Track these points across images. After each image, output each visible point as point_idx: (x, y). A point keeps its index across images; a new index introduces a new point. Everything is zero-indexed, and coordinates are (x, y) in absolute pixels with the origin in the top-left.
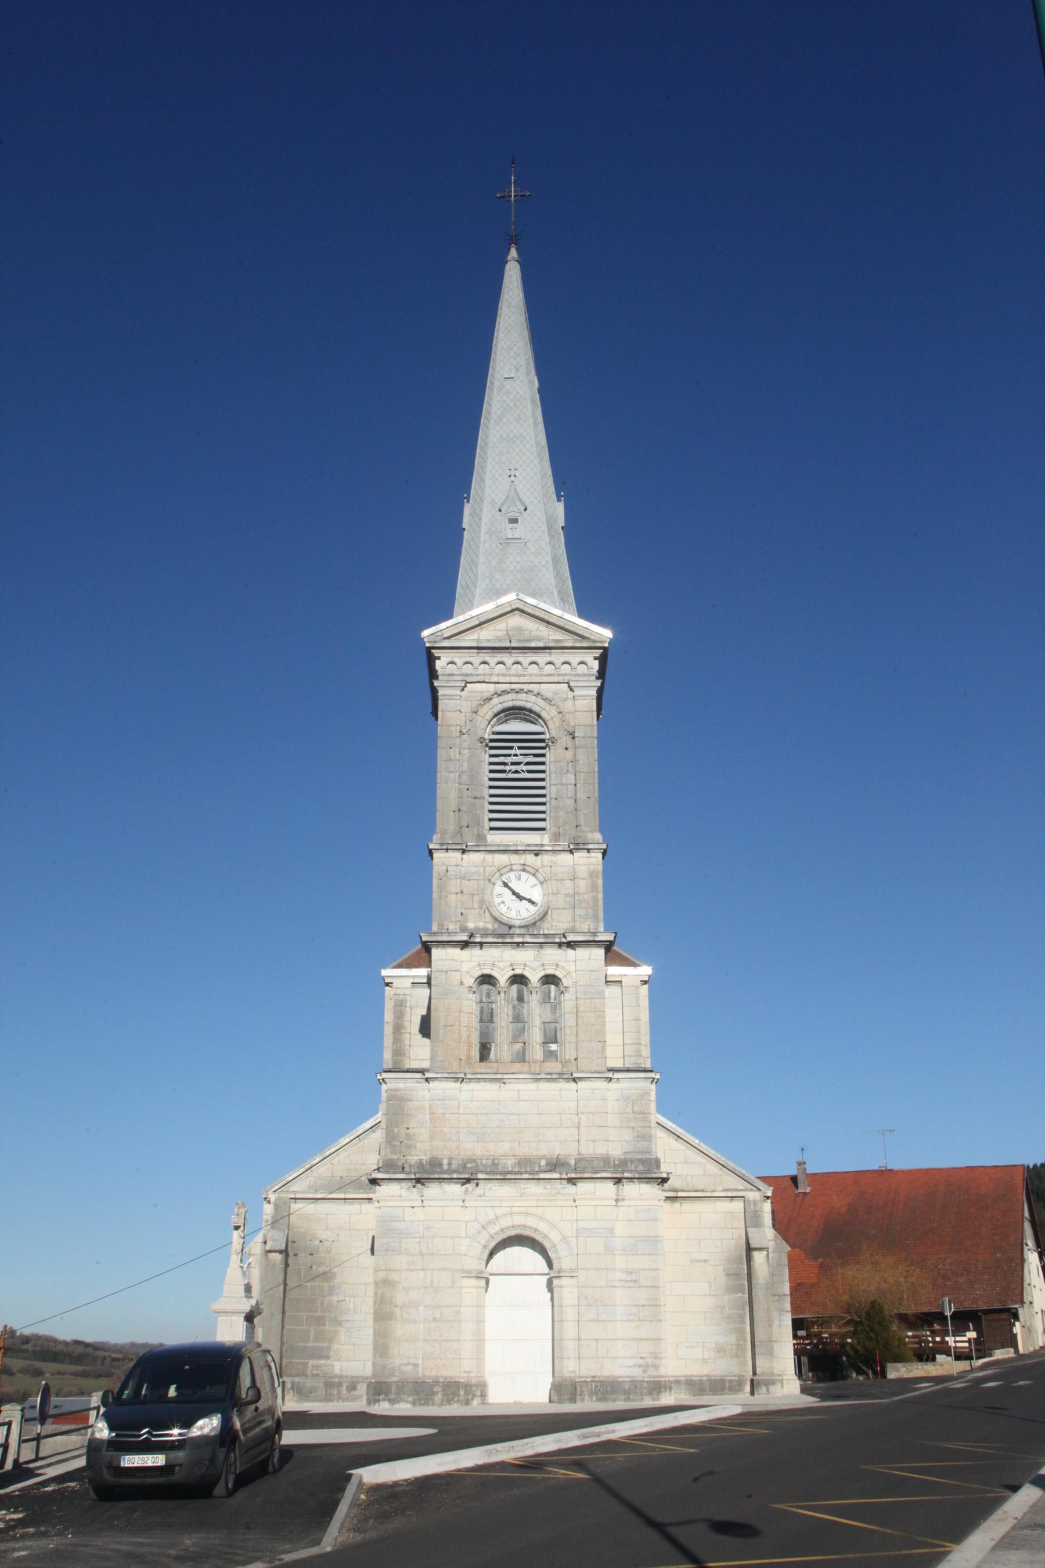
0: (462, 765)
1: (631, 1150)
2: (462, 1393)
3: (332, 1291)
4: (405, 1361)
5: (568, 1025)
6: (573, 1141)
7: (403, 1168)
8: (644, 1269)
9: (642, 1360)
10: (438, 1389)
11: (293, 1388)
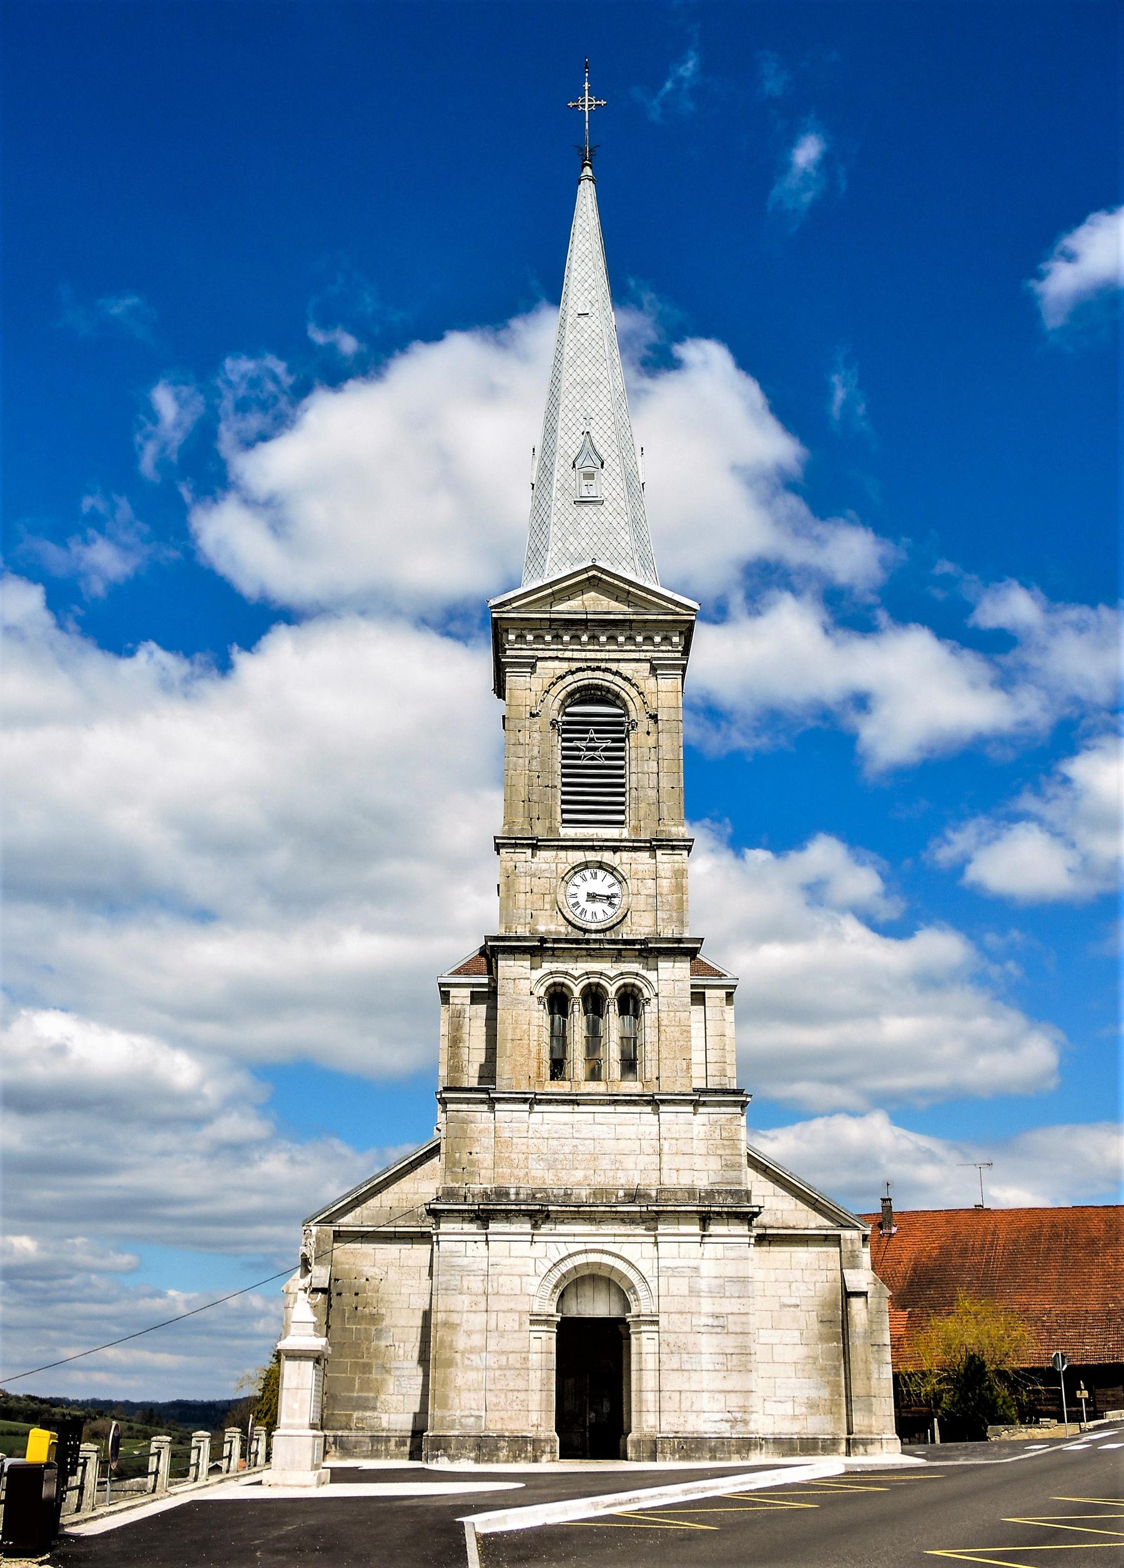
0: (532, 750)
1: (718, 1180)
2: (530, 1448)
3: (379, 1333)
4: (467, 1413)
5: (649, 1041)
6: (654, 1170)
7: (465, 1197)
8: (732, 1314)
9: (729, 1414)
10: (502, 1444)
11: (335, 1443)
